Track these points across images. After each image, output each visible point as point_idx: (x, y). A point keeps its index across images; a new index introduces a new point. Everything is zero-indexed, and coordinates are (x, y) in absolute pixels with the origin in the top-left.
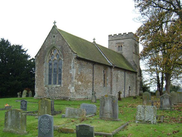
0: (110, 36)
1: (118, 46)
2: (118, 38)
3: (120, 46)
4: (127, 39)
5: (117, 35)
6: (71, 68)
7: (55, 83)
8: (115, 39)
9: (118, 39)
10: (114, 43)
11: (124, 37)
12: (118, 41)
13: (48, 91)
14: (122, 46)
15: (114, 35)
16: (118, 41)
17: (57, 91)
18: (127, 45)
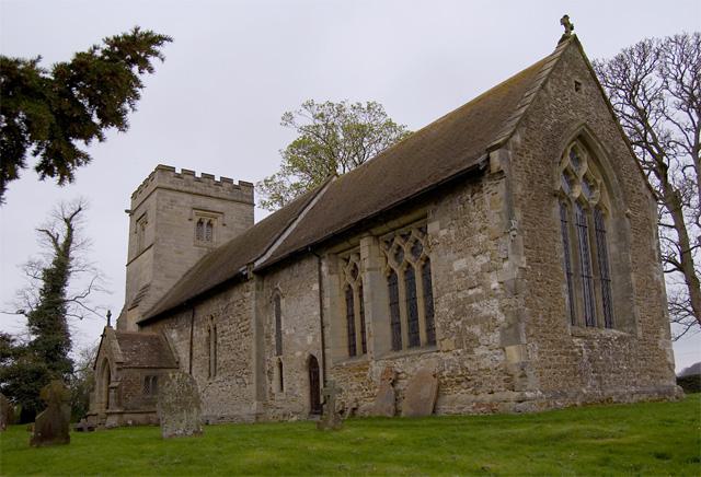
0: (162, 169)
1: (197, 219)
2: (200, 188)
4: (235, 205)
5: (198, 175)
8: (187, 189)
9: (198, 191)
12: (203, 202)
14: (215, 223)
16: (203, 202)
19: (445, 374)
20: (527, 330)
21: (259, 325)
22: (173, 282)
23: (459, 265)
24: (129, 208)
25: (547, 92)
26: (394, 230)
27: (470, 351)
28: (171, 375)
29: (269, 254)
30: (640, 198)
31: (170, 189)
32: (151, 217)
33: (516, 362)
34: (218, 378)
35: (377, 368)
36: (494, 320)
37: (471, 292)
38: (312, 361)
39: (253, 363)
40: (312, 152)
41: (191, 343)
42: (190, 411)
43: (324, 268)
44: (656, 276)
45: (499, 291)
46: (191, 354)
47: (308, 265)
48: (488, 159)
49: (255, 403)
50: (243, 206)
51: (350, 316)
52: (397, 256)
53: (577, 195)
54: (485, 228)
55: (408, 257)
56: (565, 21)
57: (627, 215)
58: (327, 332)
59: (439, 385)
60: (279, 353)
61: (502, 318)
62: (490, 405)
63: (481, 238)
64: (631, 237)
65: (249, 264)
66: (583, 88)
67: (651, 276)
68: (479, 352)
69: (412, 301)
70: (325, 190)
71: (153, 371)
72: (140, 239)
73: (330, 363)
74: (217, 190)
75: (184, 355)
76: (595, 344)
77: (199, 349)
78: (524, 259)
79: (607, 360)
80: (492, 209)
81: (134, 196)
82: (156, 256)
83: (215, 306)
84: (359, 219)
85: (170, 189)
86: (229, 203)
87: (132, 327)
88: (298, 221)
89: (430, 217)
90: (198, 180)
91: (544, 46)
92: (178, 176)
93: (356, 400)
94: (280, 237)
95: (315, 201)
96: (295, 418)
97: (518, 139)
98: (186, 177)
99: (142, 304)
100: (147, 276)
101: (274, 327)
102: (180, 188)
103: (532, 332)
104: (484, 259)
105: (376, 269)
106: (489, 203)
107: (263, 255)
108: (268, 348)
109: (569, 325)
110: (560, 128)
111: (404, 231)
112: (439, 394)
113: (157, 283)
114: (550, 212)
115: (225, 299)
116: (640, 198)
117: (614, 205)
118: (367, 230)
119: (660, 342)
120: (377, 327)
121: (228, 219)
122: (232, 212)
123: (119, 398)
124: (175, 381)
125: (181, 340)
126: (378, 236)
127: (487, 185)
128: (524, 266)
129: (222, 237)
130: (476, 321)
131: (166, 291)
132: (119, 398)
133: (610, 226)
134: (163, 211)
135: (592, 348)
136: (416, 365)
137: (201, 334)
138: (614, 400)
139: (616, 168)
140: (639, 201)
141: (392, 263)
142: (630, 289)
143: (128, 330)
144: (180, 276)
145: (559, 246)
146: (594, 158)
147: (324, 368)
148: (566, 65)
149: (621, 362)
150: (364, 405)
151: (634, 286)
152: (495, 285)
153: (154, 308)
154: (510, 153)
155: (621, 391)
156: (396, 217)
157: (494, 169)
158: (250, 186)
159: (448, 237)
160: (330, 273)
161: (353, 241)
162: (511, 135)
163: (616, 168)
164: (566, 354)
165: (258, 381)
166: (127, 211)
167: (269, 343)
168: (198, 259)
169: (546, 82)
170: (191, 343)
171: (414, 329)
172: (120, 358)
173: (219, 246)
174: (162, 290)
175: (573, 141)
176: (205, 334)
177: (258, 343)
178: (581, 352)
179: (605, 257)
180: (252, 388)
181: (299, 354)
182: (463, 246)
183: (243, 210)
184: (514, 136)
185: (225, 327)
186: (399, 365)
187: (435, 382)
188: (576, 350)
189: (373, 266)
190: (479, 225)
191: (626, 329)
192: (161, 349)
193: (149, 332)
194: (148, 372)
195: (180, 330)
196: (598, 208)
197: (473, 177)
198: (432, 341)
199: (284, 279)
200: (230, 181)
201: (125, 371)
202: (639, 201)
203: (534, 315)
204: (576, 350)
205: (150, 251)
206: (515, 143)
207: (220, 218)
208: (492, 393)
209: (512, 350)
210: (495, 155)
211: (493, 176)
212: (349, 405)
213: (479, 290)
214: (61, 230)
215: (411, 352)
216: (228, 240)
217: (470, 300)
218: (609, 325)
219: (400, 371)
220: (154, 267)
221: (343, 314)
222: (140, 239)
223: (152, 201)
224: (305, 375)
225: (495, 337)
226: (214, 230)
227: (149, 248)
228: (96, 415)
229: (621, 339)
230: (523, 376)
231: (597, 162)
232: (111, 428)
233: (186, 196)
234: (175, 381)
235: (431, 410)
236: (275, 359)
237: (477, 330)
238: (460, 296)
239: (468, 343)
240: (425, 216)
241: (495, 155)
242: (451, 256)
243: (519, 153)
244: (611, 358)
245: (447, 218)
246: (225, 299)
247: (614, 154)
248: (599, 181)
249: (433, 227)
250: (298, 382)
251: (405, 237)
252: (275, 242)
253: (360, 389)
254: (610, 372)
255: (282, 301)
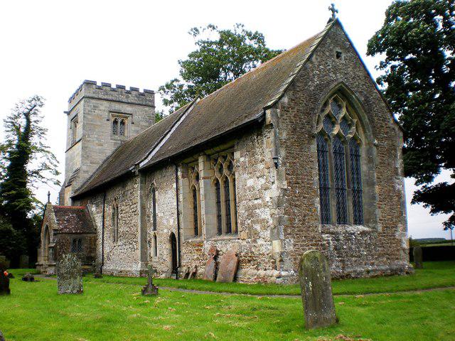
0: (89, 84)
1: (113, 120)
2: (115, 96)
3: (120, 121)
4: (141, 108)
5: (114, 86)
6: (397, 174)
7: (342, 220)
8: (106, 97)
9: (114, 99)
10: (102, 108)
11: (132, 99)
12: (117, 107)
13: (335, 249)
14: (126, 121)
15: (133, 89)
16: (117, 107)
17: (367, 246)
18: (141, 123)
19: (242, 254)
20: (285, 230)
21: (143, 208)
22: (97, 166)
23: (250, 183)
24: (67, 110)
25: (312, 63)
26: (218, 152)
27: (255, 241)
28: (64, 256)
29: (146, 161)
30: (388, 130)
31: (93, 98)
32: (80, 118)
33: (278, 251)
34: (119, 243)
35: (207, 246)
36: (267, 222)
37: (256, 202)
38: (173, 236)
39: (139, 235)
40: (207, 68)
41: (103, 216)
42: (76, 278)
43: (179, 173)
44: (398, 187)
45: (269, 204)
46: (103, 224)
47: (171, 170)
48: (264, 114)
49: (140, 264)
50: (147, 109)
51: (195, 208)
52: (221, 170)
53: (335, 132)
54: (263, 160)
55: (225, 172)
56: (333, 10)
57: (375, 145)
58: (181, 218)
59: (239, 262)
60: (155, 229)
61: (271, 222)
62: (263, 278)
63: (261, 166)
64: (377, 160)
65: (136, 165)
66: (343, 56)
67: (393, 187)
68: (260, 242)
69: (227, 201)
70: (191, 109)
71: (78, 236)
72: (74, 133)
73: (182, 239)
74: (127, 97)
75: (99, 224)
76: (341, 238)
77: (108, 222)
78: (285, 183)
79: (350, 248)
80: (267, 148)
81: (70, 101)
82: (84, 148)
83: (118, 192)
84: (167, 156)
85: (93, 98)
86: (137, 107)
87: (68, 203)
88: (171, 133)
89: (236, 148)
90: (114, 90)
91: (318, 26)
92: (99, 88)
93: (196, 267)
94: (157, 145)
95: (184, 117)
96: (164, 275)
97: (286, 100)
98: (104, 88)
99: (74, 183)
100: (78, 162)
101: (152, 210)
102: (100, 96)
103: (289, 231)
104: (262, 181)
105: (208, 178)
106: (266, 147)
107: (145, 159)
108: (148, 224)
109: (320, 226)
110: (320, 88)
111: (223, 154)
112: (238, 267)
113: (84, 168)
114: (309, 148)
115: (123, 187)
116: (388, 130)
117: (366, 137)
118: (203, 151)
119: (397, 234)
120: (207, 216)
121: (135, 117)
122: (139, 113)
123: (56, 255)
124: (66, 260)
125: (98, 213)
126: (187, 164)
127: (265, 132)
128: (286, 187)
129: (131, 132)
130: (257, 222)
131: (91, 174)
132: (56, 255)
133: (363, 152)
134: (88, 114)
135: (338, 240)
136: (229, 246)
137: (109, 210)
138: (353, 276)
139: (369, 111)
140: (387, 133)
141: (217, 175)
142: (374, 198)
143: (66, 205)
144: (101, 162)
145: (316, 171)
146: (351, 105)
147: (179, 243)
148: (329, 41)
149: (362, 249)
150: (200, 270)
151: (377, 195)
152: (268, 199)
153: (82, 186)
154: (278, 110)
155: (359, 269)
156: (212, 147)
157: (268, 123)
158: (152, 93)
159: (244, 162)
160: (183, 177)
161: (195, 157)
162: (280, 98)
163: (369, 111)
164: (317, 245)
165: (142, 248)
166: (65, 112)
167: (149, 221)
168: (114, 149)
169: (311, 56)
170: (103, 216)
171: (227, 225)
172: (56, 226)
173: (128, 140)
174: (88, 173)
175: (334, 94)
176: (111, 211)
177: (142, 221)
178: (329, 243)
179: (358, 174)
180: (139, 252)
181: (165, 231)
182: (251, 169)
183: (146, 111)
184: (283, 98)
185: (123, 207)
186: (219, 246)
187: (236, 259)
188: (325, 242)
189: (207, 176)
190: (260, 158)
191: (370, 225)
192: (84, 218)
193: (78, 206)
194: (74, 236)
195: (97, 206)
196: (355, 139)
197: (256, 128)
198: (236, 232)
199: (157, 180)
200: (136, 90)
201: (59, 235)
202: (387, 133)
203: (291, 220)
204: (325, 242)
205: (80, 144)
206: (284, 103)
207: (130, 118)
208: (265, 270)
209: (276, 243)
210: (268, 112)
211: (267, 127)
212: (192, 270)
213: (259, 201)
214: (22, 122)
215: (226, 237)
216: (136, 135)
217: (255, 207)
218: (358, 221)
219: (219, 249)
220: (83, 156)
221: (191, 206)
222: (74, 133)
223: (81, 106)
224: (168, 246)
225: (267, 233)
226: (126, 127)
227: (80, 141)
228: (42, 265)
229: (363, 233)
230: (281, 261)
231: (353, 107)
232: (50, 275)
233: (105, 102)
234: (66, 260)
235: (232, 278)
236: (152, 233)
237: (258, 227)
238: (250, 204)
239: (254, 236)
240: (233, 147)
241: (268, 112)
242: (246, 176)
243: (285, 109)
244: (353, 247)
245: (244, 150)
246: (123, 187)
247: (367, 100)
248: (355, 120)
249: (237, 155)
250: (165, 249)
251: (225, 157)
252: (154, 148)
253: (198, 259)
254: (352, 256)
255: (157, 193)
